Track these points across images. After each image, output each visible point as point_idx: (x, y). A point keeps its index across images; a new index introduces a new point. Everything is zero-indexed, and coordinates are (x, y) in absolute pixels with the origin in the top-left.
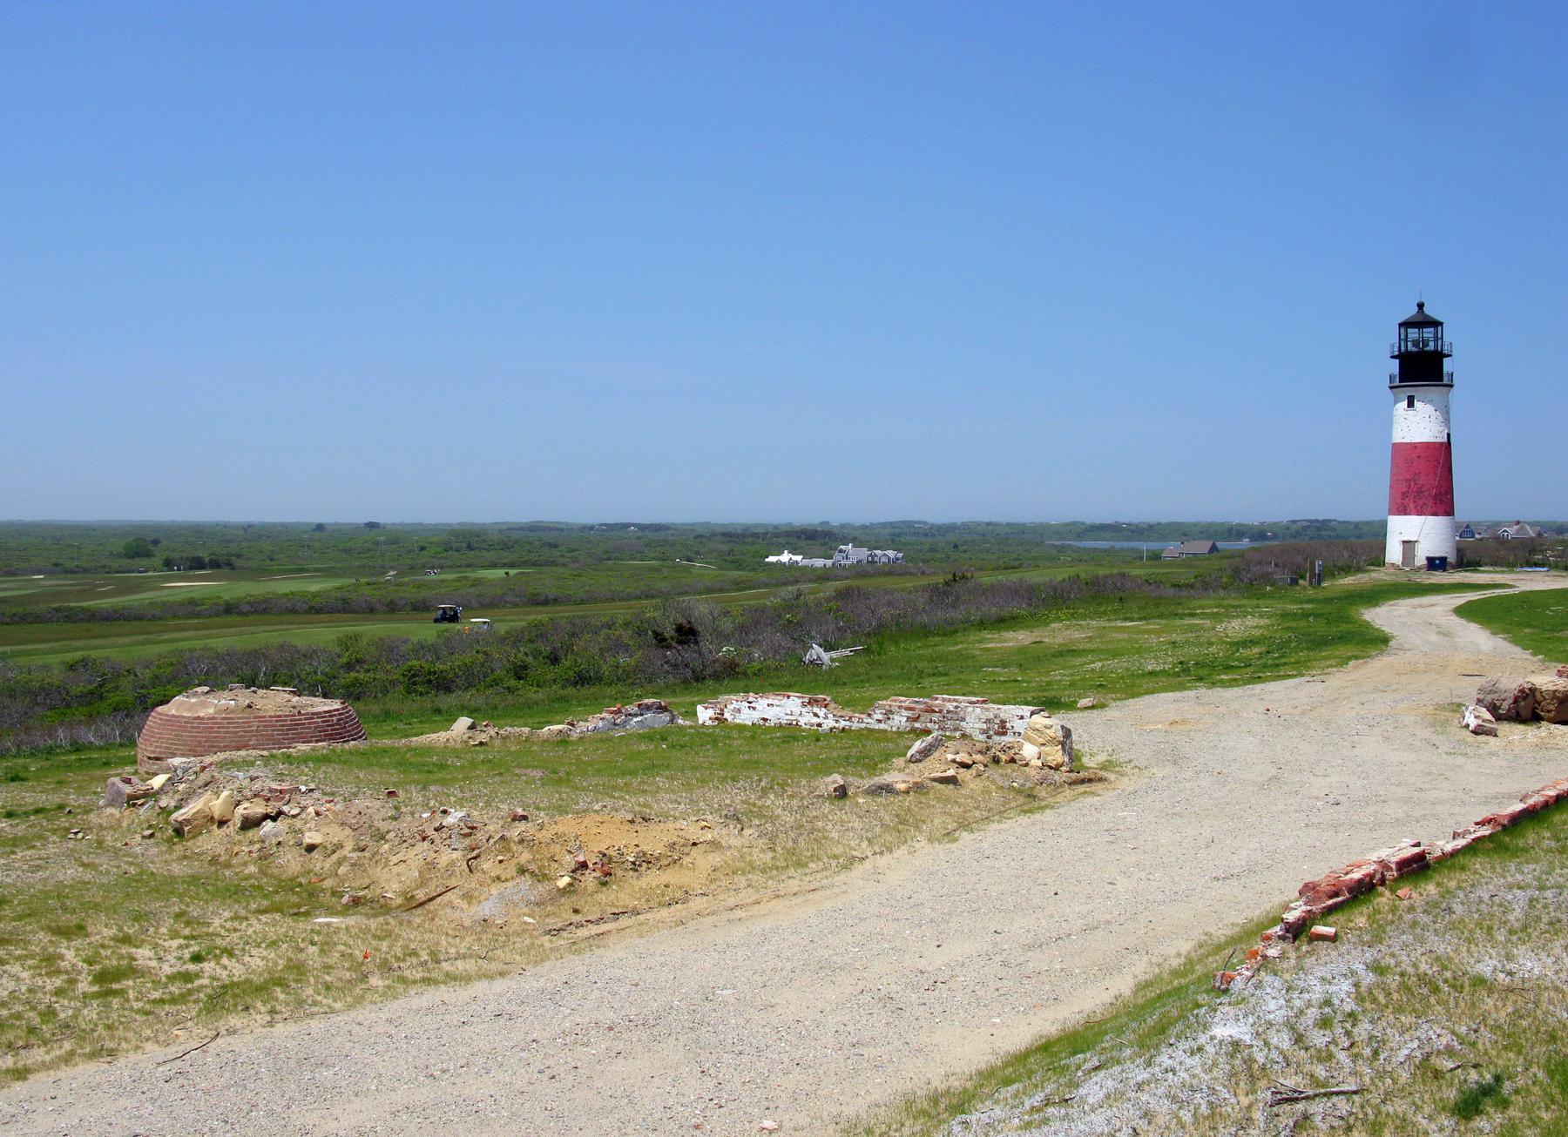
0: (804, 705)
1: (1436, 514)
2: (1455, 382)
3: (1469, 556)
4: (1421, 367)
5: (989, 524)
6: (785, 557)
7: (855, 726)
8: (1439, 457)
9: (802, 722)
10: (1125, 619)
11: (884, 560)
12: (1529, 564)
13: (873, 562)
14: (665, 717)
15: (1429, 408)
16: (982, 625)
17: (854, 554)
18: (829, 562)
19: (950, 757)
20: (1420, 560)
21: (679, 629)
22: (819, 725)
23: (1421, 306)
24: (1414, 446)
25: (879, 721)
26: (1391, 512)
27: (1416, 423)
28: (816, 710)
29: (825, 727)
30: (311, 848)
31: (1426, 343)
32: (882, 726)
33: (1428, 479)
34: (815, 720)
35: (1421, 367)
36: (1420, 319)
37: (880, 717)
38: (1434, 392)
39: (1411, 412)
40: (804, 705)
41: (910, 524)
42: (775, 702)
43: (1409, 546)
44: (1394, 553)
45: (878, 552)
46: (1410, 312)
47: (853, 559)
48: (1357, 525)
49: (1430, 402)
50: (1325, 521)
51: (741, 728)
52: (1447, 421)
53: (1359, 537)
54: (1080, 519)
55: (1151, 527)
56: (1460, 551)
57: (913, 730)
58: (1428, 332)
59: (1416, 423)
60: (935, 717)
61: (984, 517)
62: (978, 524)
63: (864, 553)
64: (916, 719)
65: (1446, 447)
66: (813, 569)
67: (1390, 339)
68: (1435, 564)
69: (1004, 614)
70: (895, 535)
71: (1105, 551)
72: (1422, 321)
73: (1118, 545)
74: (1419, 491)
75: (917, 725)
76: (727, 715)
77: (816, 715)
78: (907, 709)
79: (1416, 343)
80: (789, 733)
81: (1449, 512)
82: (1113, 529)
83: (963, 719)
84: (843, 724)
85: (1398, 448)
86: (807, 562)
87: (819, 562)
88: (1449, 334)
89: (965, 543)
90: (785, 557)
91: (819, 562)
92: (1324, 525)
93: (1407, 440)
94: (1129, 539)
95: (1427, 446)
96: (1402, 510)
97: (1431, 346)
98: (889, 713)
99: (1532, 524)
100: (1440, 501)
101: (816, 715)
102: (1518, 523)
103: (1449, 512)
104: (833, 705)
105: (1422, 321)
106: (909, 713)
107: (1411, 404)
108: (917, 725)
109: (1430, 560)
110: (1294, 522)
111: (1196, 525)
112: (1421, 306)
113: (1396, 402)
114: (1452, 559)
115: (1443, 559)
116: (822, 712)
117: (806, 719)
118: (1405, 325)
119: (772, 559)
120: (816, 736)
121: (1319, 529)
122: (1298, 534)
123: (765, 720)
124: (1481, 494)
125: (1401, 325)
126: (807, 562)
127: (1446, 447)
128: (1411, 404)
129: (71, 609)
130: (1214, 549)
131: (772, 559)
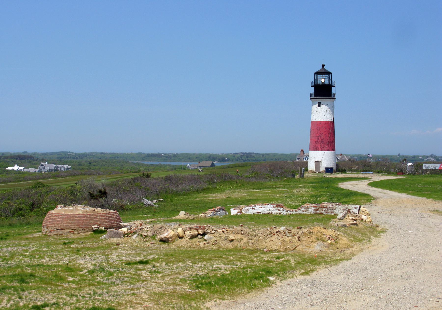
0: (274, 207)
1: (328, 150)
3: (342, 167)
4: (323, 92)
5: (102, 153)
6: (16, 168)
7: (294, 213)
8: (330, 127)
9: (273, 212)
10: (254, 189)
11: (62, 169)
12: (364, 171)
13: (57, 170)
14: (224, 212)
16: (198, 191)
17: (48, 166)
18: (37, 170)
19: (351, 218)
20: (323, 169)
21: (100, 192)
22: (280, 213)
23: (323, 66)
24: (320, 123)
25: (303, 211)
26: (311, 149)
27: (321, 113)
28: (279, 208)
29: (282, 214)
30: (232, 240)
32: (304, 213)
33: (325, 135)
34: (279, 212)
36: (323, 71)
37: (304, 210)
38: (328, 101)
39: (319, 109)
40: (274, 207)
41: (66, 153)
42: (263, 206)
44: (312, 166)
45: (59, 166)
46: (319, 68)
48: (263, 155)
49: (327, 105)
50: (249, 153)
51: (250, 215)
53: (265, 160)
54: (142, 151)
55: (175, 155)
56: (337, 165)
57: (316, 213)
59: (321, 113)
60: (324, 209)
61: (99, 151)
62: (97, 153)
63: (52, 166)
64: (317, 210)
67: (311, 79)
68: (328, 170)
70: (61, 158)
71: (157, 165)
72: (324, 72)
73: (162, 163)
74: (322, 141)
75: (318, 212)
76: (243, 211)
77: (279, 210)
78: (314, 207)
80: (268, 215)
81: (334, 150)
82: (158, 156)
83: (335, 209)
84: (290, 212)
85: (313, 123)
86: (26, 170)
87: (32, 170)
88: (334, 78)
89: (94, 162)
90: (16, 168)
91: (32, 170)
92: (249, 155)
94: (165, 160)
95: (325, 123)
96: (315, 148)
98: (307, 209)
99: (347, 156)
100: (330, 145)
101: (279, 210)
102: (341, 155)
103: (334, 150)
104: (284, 207)
105: (324, 72)
106: (315, 208)
107: (319, 106)
108: (318, 212)
110: (236, 154)
111: (194, 154)
112: (323, 66)
113: (313, 105)
114: (335, 169)
115: (332, 169)
116: (281, 209)
117: (275, 211)
119: (10, 168)
120: (280, 216)
121: (247, 157)
122: (237, 160)
123: (258, 212)
124: (349, 143)
125: (315, 73)
128: (319, 106)
130: (213, 165)
131: (10, 168)
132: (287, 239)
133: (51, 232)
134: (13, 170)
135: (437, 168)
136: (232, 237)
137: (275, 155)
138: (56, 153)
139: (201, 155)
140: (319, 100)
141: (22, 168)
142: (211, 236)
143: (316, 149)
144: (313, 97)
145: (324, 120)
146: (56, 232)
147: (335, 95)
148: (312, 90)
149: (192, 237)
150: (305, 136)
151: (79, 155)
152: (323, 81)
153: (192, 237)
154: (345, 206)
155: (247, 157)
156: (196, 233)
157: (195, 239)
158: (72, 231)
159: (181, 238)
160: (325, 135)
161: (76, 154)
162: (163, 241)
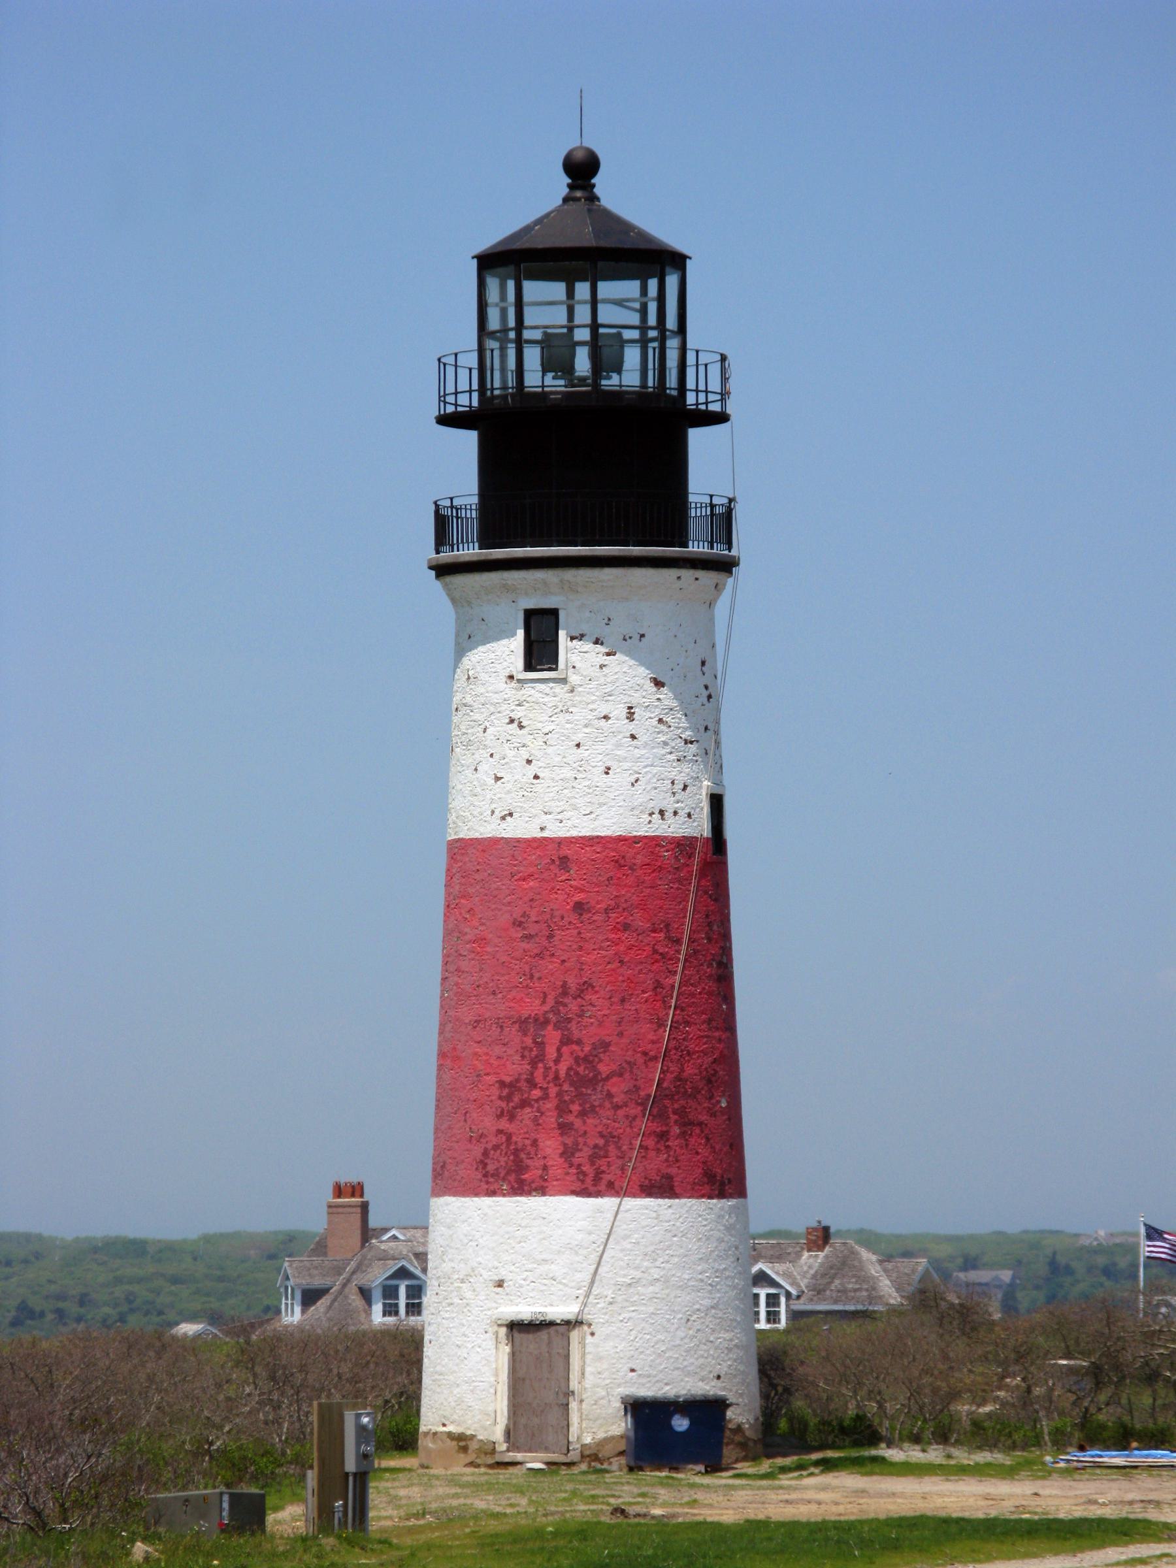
1: (660, 1187)
2: (744, 543)
4: (583, 472)
8: (670, 904)
15: (627, 675)
20: (598, 1418)
23: (582, 170)
24: (559, 854)
26: (447, 1180)
27: (564, 746)
31: (605, 353)
33: (616, 1017)
35: (583, 472)
36: (584, 236)
38: (646, 594)
39: (541, 692)
43: (538, 1342)
44: (466, 1385)
46: (531, 198)
49: (631, 642)
52: (706, 736)
54: (1070, 1225)
56: (772, 1366)
58: (620, 299)
59: (564, 746)
65: (695, 872)
66: (420, 1526)
67: (435, 329)
68: (668, 1433)
74: (585, 1079)
79: (557, 354)
81: (723, 1177)
85: (472, 861)
88: (723, 321)
93: (521, 828)
95: (618, 853)
96: (508, 1171)
97: (629, 376)
99: (894, 1250)
102: (822, 1236)
103: (723, 1177)
107: (540, 652)
109: (647, 1414)
112: (582, 170)
113: (466, 641)
114: (742, 1414)
115: (708, 1412)
118: (505, 262)
124: (919, 1092)
125: (488, 262)
127: (695, 872)
128: (540, 652)
143: (513, 1174)
144: (471, 551)
147: (723, 522)
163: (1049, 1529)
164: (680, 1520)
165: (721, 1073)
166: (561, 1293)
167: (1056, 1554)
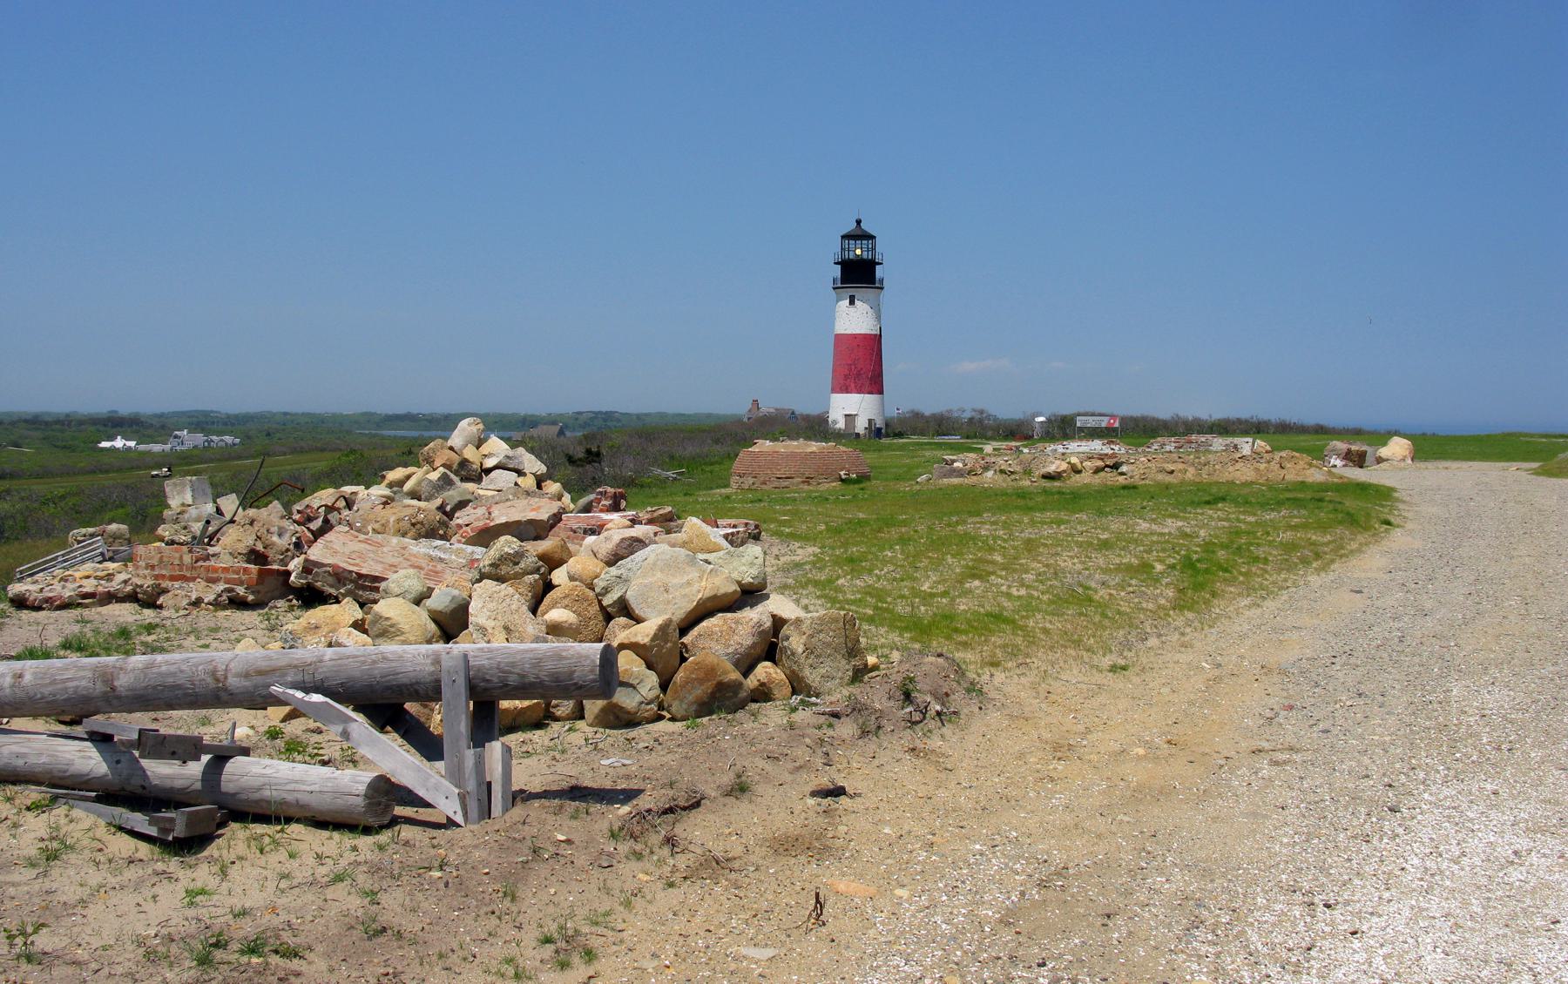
4: (858, 274)
5: (285, 414)
6: (119, 443)
8: (871, 346)
23: (859, 222)
24: (855, 336)
26: (834, 391)
27: (854, 318)
33: (862, 364)
38: (870, 293)
39: (852, 309)
46: (850, 226)
47: (189, 445)
52: (878, 318)
59: (854, 318)
63: (199, 439)
67: (833, 249)
69: (176, 538)
72: (859, 235)
74: (859, 374)
81: (881, 392)
85: (837, 336)
86: (142, 447)
87: (157, 448)
90: (119, 443)
91: (157, 448)
95: (865, 337)
100: (874, 384)
103: (881, 392)
105: (859, 235)
107: (852, 302)
110: (580, 413)
112: (859, 222)
119: (105, 444)
121: (605, 420)
124: (914, 384)
126: (142, 447)
128: (852, 302)
129: (383, 438)
131: (105, 444)
132: (1262, 466)
133: (764, 483)
134: (113, 450)
135: (1104, 425)
136: (1170, 467)
137: (662, 415)
138: (183, 413)
139: (503, 416)
140: (851, 292)
141: (132, 444)
142: (1131, 467)
143: (847, 390)
145: (863, 332)
146: (776, 484)
147: (882, 281)
148: (837, 271)
149: (1097, 470)
150: (824, 363)
151: (237, 416)
152: (858, 252)
153: (1097, 470)
154: (1229, 440)
155: (605, 420)
156: (1100, 463)
157: (1102, 474)
158: (808, 481)
159: (1079, 472)
160: (862, 364)
161: (228, 416)
162: (1048, 477)
163: (812, 428)
164: (1535, 465)
165: (880, 375)
166: (851, 408)
167: (172, 789)
